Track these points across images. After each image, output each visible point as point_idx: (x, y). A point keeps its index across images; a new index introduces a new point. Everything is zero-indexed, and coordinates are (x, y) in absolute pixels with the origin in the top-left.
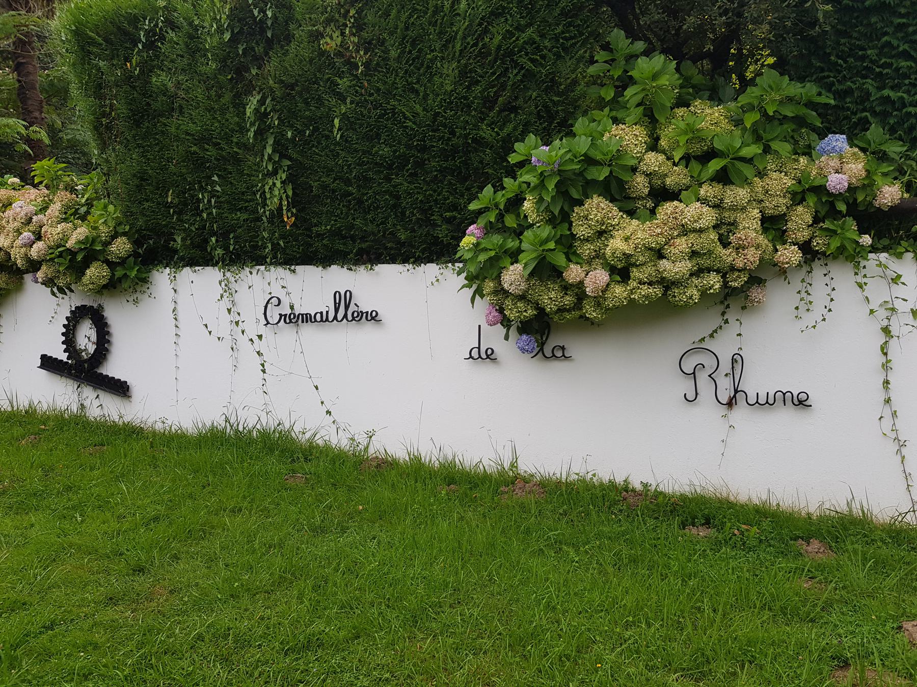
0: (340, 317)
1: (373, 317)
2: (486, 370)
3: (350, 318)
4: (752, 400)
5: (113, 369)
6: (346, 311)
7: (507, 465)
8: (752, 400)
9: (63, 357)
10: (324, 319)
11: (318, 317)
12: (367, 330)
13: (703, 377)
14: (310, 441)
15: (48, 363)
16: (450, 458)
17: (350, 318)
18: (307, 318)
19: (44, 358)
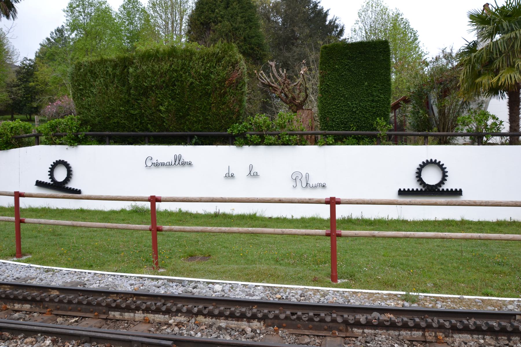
0: (177, 163)
1: (190, 164)
2: (230, 181)
3: (181, 164)
4: (311, 186)
5: (71, 185)
6: (179, 162)
7: (350, 216)
8: (311, 186)
9: (66, 186)
10: (169, 165)
11: (168, 164)
12: (186, 169)
13: (298, 181)
14: (375, 219)
15: (39, 184)
16: (325, 10)
17: (181, 164)
18: (163, 164)
19: (37, 182)
